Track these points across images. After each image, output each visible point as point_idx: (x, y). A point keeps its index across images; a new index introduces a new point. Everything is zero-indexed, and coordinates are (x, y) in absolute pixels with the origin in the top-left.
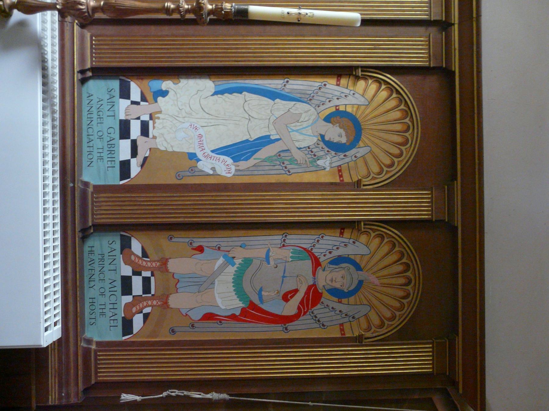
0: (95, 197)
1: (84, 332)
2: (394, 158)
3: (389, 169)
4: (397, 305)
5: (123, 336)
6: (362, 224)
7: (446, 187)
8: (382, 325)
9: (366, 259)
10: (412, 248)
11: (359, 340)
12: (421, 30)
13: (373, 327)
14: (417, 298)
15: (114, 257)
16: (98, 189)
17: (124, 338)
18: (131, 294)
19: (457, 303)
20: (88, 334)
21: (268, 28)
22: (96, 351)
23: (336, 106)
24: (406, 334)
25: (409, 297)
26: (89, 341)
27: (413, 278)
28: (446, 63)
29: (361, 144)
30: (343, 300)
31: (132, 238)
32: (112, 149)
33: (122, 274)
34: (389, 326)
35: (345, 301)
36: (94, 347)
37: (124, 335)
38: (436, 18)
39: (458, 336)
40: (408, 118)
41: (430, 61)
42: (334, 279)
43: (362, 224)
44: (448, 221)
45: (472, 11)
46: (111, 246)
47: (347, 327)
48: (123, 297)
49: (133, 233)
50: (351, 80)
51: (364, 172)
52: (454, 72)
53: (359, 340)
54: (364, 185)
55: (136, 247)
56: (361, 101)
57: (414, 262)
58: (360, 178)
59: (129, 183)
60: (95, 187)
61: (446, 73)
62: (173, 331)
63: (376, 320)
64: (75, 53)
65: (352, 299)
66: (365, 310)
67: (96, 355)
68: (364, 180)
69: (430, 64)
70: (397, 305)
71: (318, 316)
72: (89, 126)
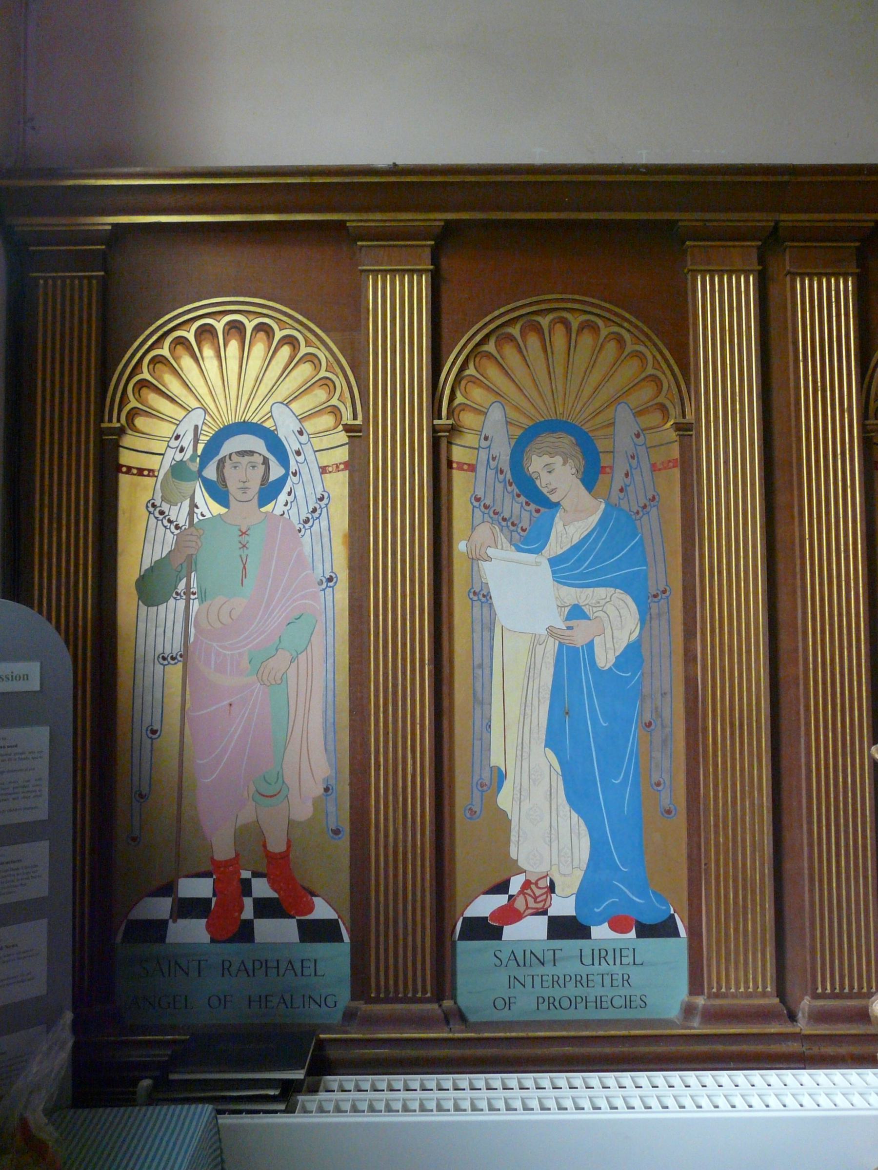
0: (405, 995)
1: (668, 1023)
2: (626, 353)
4: (286, 351)
5: (342, 941)
6: (436, 422)
7: (359, 243)
8: (326, 383)
9: (513, 415)
11: (685, 430)
12: (774, 291)
16: (696, 985)
17: (346, 937)
18: (551, 919)
19: (644, 223)
20: (673, 1012)
21: (783, 617)
22: (709, 997)
24: (673, 332)
26: (688, 1010)
27: (585, 317)
28: (426, 239)
29: (269, 424)
30: (603, 463)
32: (527, 957)
33: (544, 936)
35: (605, 461)
36: (700, 1001)
37: (676, 934)
38: (428, 260)
39: (678, 221)
41: (420, 272)
42: (241, 485)
43: (436, 422)
44: (857, 240)
45: (393, 183)
47: (326, 459)
48: (503, 939)
49: (458, 912)
50: (128, 440)
51: (327, 421)
52: (447, 222)
53: (685, 430)
54: (355, 417)
55: (485, 906)
58: (341, 428)
59: (348, 924)
60: (354, 998)
61: (445, 239)
62: (337, 832)
64: (393, 1036)
65: (601, 445)
67: (823, 996)
68: (344, 418)
69: (426, 271)
70: (286, 351)
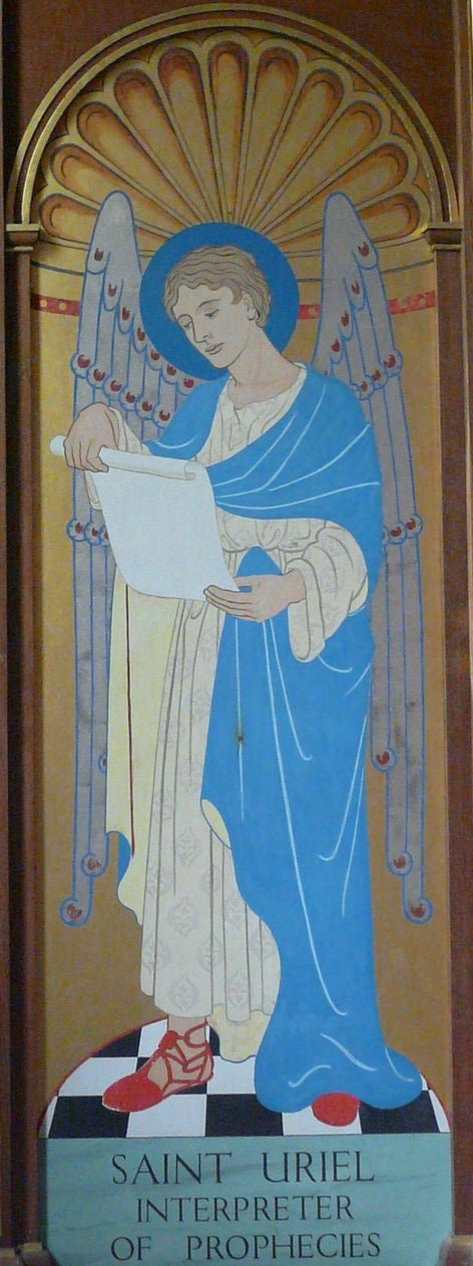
2: (344, 106)
3: (386, 127)
10: (127, 31)
13: (402, 188)
14: (285, 21)
15: (172, 1160)
23: (318, 308)
25: (239, 46)
31: (62, 1094)
32: (171, 1165)
33: (201, 1130)
34: (398, 128)
40: (192, 46)
46: (131, 1176)
55: (95, 1078)
56: (116, 213)
57: (278, 28)
59: (449, 1094)
63: (380, 175)
66: (339, 214)
71: (359, 380)
72: (223, 1252)
